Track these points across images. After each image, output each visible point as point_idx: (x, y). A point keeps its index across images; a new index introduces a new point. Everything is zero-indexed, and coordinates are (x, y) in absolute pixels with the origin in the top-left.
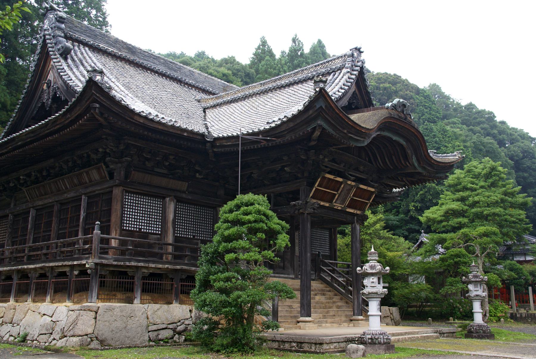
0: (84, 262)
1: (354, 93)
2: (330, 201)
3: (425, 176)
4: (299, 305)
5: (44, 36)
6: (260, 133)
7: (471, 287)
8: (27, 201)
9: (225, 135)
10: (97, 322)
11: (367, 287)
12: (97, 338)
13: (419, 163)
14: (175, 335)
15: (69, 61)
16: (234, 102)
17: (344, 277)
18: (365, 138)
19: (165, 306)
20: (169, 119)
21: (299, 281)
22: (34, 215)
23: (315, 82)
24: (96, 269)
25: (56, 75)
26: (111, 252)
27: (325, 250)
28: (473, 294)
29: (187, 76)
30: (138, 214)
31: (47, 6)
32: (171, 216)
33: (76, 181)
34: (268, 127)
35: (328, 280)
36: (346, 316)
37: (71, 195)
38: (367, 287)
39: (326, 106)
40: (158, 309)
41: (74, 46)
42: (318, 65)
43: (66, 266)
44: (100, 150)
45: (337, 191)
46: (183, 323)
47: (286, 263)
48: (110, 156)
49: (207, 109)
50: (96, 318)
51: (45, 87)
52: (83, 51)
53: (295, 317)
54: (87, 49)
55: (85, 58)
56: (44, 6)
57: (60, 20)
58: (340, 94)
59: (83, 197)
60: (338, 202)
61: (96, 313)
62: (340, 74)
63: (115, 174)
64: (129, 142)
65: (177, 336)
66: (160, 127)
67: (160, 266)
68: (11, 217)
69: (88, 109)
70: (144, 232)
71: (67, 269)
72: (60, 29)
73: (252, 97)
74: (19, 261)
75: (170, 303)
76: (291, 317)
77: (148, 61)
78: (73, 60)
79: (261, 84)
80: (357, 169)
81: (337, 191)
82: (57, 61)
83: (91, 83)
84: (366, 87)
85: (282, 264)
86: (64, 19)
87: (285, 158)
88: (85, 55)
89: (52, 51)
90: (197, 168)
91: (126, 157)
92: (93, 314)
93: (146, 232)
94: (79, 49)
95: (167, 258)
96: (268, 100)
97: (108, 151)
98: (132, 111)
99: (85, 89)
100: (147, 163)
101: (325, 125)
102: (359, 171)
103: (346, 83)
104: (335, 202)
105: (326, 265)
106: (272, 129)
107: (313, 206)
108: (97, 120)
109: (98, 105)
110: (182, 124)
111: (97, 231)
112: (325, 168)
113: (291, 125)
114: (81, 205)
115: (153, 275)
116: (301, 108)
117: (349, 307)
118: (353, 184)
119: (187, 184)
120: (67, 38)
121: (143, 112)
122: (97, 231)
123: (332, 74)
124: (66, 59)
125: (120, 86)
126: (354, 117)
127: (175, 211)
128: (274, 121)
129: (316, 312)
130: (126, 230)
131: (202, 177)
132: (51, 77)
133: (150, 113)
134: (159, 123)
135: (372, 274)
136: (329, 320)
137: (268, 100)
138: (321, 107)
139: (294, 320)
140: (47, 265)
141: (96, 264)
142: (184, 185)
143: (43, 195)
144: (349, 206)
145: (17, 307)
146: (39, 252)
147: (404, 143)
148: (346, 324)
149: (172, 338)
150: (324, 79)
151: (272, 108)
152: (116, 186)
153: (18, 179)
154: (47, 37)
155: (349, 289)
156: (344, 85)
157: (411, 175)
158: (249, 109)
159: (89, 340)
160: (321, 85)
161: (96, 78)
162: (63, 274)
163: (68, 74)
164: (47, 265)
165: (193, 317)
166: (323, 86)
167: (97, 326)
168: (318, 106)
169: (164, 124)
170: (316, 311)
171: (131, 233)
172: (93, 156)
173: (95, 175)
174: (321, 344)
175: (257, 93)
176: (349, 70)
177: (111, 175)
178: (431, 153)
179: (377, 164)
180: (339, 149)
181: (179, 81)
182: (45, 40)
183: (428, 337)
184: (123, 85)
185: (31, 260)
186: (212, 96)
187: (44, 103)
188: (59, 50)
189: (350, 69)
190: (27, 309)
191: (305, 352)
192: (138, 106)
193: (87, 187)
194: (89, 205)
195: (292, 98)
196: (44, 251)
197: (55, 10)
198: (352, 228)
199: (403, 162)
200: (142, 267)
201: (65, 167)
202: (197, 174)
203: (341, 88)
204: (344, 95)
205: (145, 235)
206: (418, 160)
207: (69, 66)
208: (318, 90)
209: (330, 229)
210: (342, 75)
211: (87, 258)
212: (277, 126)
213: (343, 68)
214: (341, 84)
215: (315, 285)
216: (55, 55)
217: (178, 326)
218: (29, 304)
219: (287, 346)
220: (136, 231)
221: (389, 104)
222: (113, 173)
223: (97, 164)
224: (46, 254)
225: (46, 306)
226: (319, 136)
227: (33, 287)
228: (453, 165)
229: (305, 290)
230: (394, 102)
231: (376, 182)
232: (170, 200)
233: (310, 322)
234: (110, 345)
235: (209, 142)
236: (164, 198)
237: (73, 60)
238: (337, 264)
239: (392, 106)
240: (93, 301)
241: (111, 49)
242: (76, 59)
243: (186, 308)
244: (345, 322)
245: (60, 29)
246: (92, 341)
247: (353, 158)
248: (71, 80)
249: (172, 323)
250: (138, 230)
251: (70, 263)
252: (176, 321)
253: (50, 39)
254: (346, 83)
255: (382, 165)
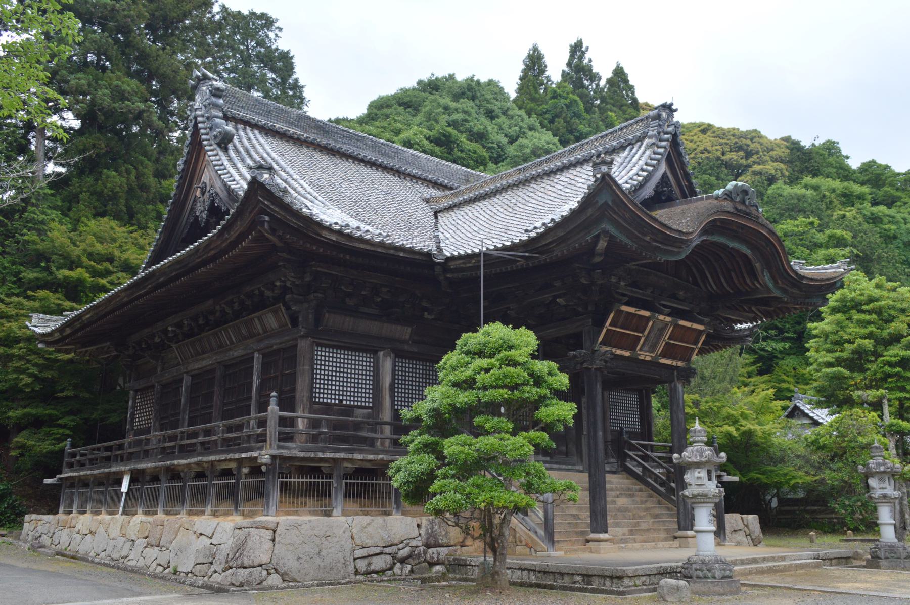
0: (255, 454)
1: (664, 176)
2: (632, 348)
3: (786, 303)
4: (589, 513)
5: (195, 118)
6: (514, 247)
7: (872, 482)
8: (179, 364)
9: (462, 252)
10: (276, 546)
11: (690, 485)
12: (276, 570)
13: (776, 282)
14: (395, 564)
15: (232, 153)
16: (479, 200)
17: (663, 467)
18: (681, 248)
19: (379, 520)
20: (378, 232)
21: (587, 474)
22: (189, 384)
23: (595, 165)
24: (273, 464)
25: (213, 174)
26: (297, 437)
27: (632, 423)
28: (877, 494)
29: (408, 163)
30: (338, 376)
31: (199, 74)
32: (387, 380)
33: (244, 331)
34: (525, 237)
35: (638, 471)
36: (668, 531)
37: (237, 353)
38: (690, 485)
39: (613, 201)
40: (368, 524)
41: (237, 130)
42: (606, 135)
43: (230, 460)
44: (278, 283)
45: (642, 332)
46: (407, 545)
47: (570, 446)
48: (292, 293)
49: (440, 211)
50: (273, 540)
51: (198, 193)
52: (251, 136)
53: (583, 533)
54: (256, 132)
55: (253, 146)
56: (194, 75)
57: (217, 93)
58: (641, 179)
59: (256, 355)
60: (646, 348)
61: (275, 532)
62: (640, 147)
63: (300, 319)
64: (319, 269)
65: (398, 565)
66: (362, 246)
67: (371, 457)
68: (158, 387)
69: (254, 224)
70: (346, 406)
71: (233, 465)
72: (216, 106)
73: (506, 191)
74: (167, 453)
75: (387, 514)
76: (577, 533)
77: (347, 144)
78: (237, 151)
79: (520, 170)
80: (674, 297)
81: (642, 332)
82: (213, 154)
83: (255, 185)
84: (683, 165)
85: (563, 447)
86: (222, 91)
87: (557, 284)
88: (255, 142)
89: (207, 140)
90: (425, 304)
91: (315, 292)
92: (269, 533)
93: (350, 406)
94: (246, 133)
95: (382, 444)
96: (531, 194)
97: (288, 284)
98: (320, 225)
99: (248, 193)
100: (347, 300)
101: (613, 231)
102: (678, 299)
103: (649, 161)
104: (641, 350)
105: (633, 448)
106: (532, 240)
107: (603, 357)
108: (268, 239)
109: (267, 218)
110: (398, 240)
111: (273, 407)
112: (621, 297)
113: (561, 233)
114: (253, 367)
115: (361, 472)
116: (574, 205)
117: (671, 516)
118: (668, 319)
119: (410, 329)
120: (226, 118)
121: (336, 224)
122: (273, 407)
123: (628, 148)
124: (226, 150)
125: (306, 185)
126: (661, 214)
127: (394, 371)
128: (535, 228)
129: (617, 525)
130: (319, 403)
131: (433, 317)
132: (205, 178)
133: (347, 226)
134: (361, 239)
135: (698, 465)
136: (638, 537)
137: (531, 194)
138: (606, 203)
139: (582, 539)
140: (205, 459)
141: (273, 457)
142: (405, 332)
143: (200, 355)
144: (664, 355)
145: (166, 523)
146: (194, 441)
147: (748, 252)
148: (667, 544)
149: (391, 568)
150: (608, 159)
151: (536, 206)
152: (302, 337)
153: (165, 331)
154: (200, 119)
155: (672, 487)
156: (646, 164)
157: (766, 302)
158: (502, 210)
159: (265, 573)
160: (604, 169)
161: (262, 177)
162: (227, 473)
163: (228, 173)
164: (205, 459)
165: (423, 534)
166: (606, 170)
167: (276, 552)
168: (601, 202)
169: (368, 242)
170: (617, 523)
171: (327, 408)
172: (268, 293)
173: (271, 321)
174: (620, 578)
175: (514, 185)
176: (653, 140)
177: (294, 321)
178: (797, 265)
179: (706, 287)
180: (642, 265)
181: (397, 173)
182: (196, 125)
183: (802, 566)
184: (311, 184)
185: (186, 451)
186: (447, 192)
187: (197, 217)
188: (216, 137)
189: (656, 138)
190: (177, 526)
191: (594, 591)
192: (330, 214)
193: (260, 340)
194: (265, 367)
195: (567, 190)
196: (201, 439)
197: (210, 79)
198: (671, 389)
199: (748, 281)
200: (344, 459)
201: (228, 310)
202: (426, 313)
203: (642, 170)
204: (646, 180)
205: (348, 410)
206: (773, 277)
207: (231, 160)
208: (598, 176)
209: (640, 392)
210: (643, 148)
211: (261, 449)
212: (540, 236)
213: (644, 138)
214: (641, 163)
215: (614, 481)
216: (211, 145)
217: (399, 550)
218: (183, 517)
219: (567, 581)
220: (335, 405)
221: (720, 192)
222: (298, 318)
223: (274, 305)
224: (203, 443)
225: (204, 522)
226: (607, 248)
227: (187, 492)
228: (835, 283)
229: (597, 491)
230: (727, 187)
231: (706, 316)
232: (385, 356)
233: (606, 541)
234: (294, 580)
235: (438, 264)
236: (375, 352)
237: (237, 151)
238: (652, 446)
239: (725, 193)
240: (270, 512)
241: (292, 131)
242: (241, 149)
243: (411, 521)
244: (666, 539)
245: (216, 106)
246: (269, 574)
247: (667, 277)
248: (234, 180)
249: (391, 546)
250: (337, 402)
251: (237, 456)
252: (396, 542)
253: (204, 123)
254: (649, 161)
255: (715, 287)
